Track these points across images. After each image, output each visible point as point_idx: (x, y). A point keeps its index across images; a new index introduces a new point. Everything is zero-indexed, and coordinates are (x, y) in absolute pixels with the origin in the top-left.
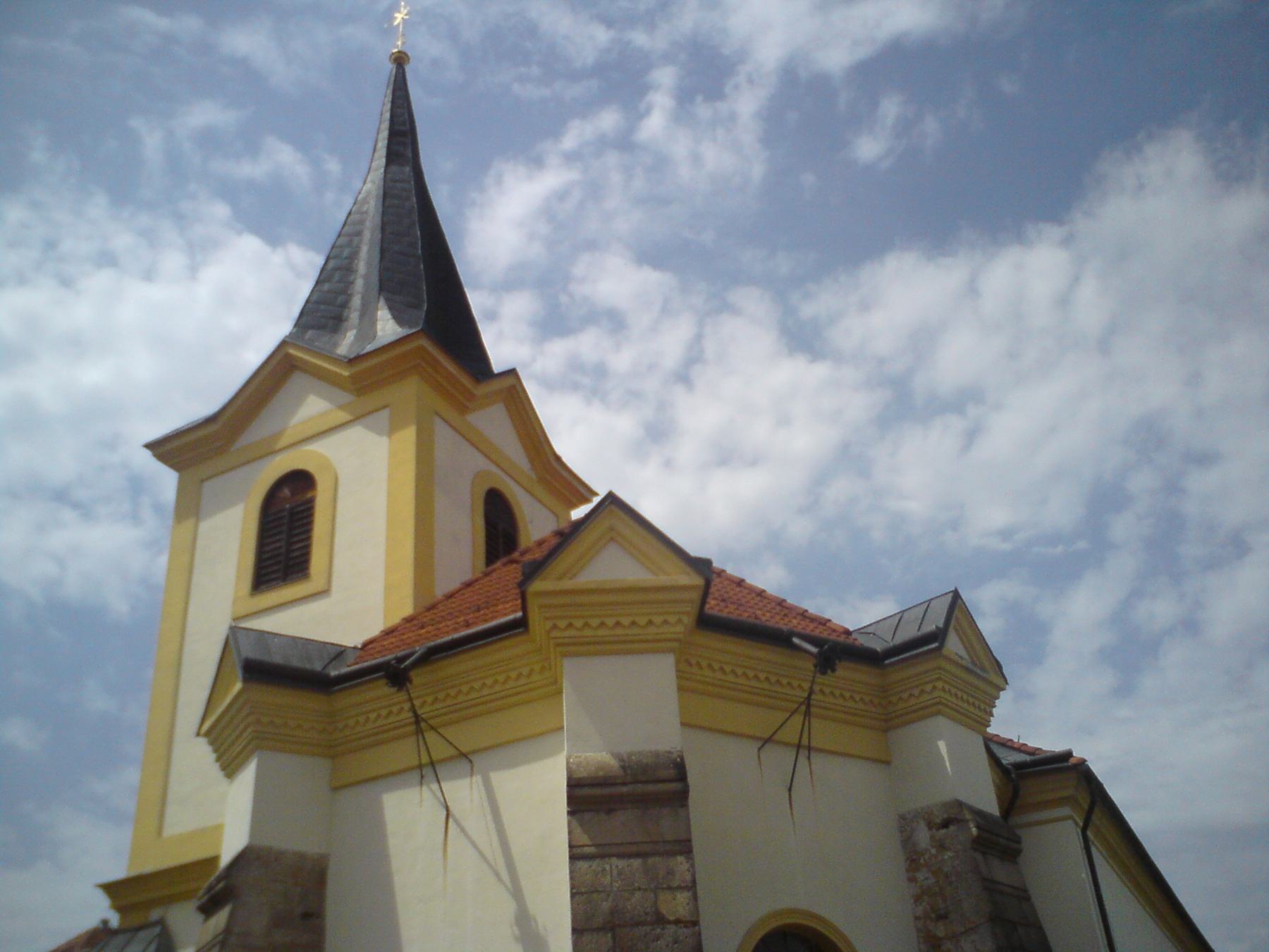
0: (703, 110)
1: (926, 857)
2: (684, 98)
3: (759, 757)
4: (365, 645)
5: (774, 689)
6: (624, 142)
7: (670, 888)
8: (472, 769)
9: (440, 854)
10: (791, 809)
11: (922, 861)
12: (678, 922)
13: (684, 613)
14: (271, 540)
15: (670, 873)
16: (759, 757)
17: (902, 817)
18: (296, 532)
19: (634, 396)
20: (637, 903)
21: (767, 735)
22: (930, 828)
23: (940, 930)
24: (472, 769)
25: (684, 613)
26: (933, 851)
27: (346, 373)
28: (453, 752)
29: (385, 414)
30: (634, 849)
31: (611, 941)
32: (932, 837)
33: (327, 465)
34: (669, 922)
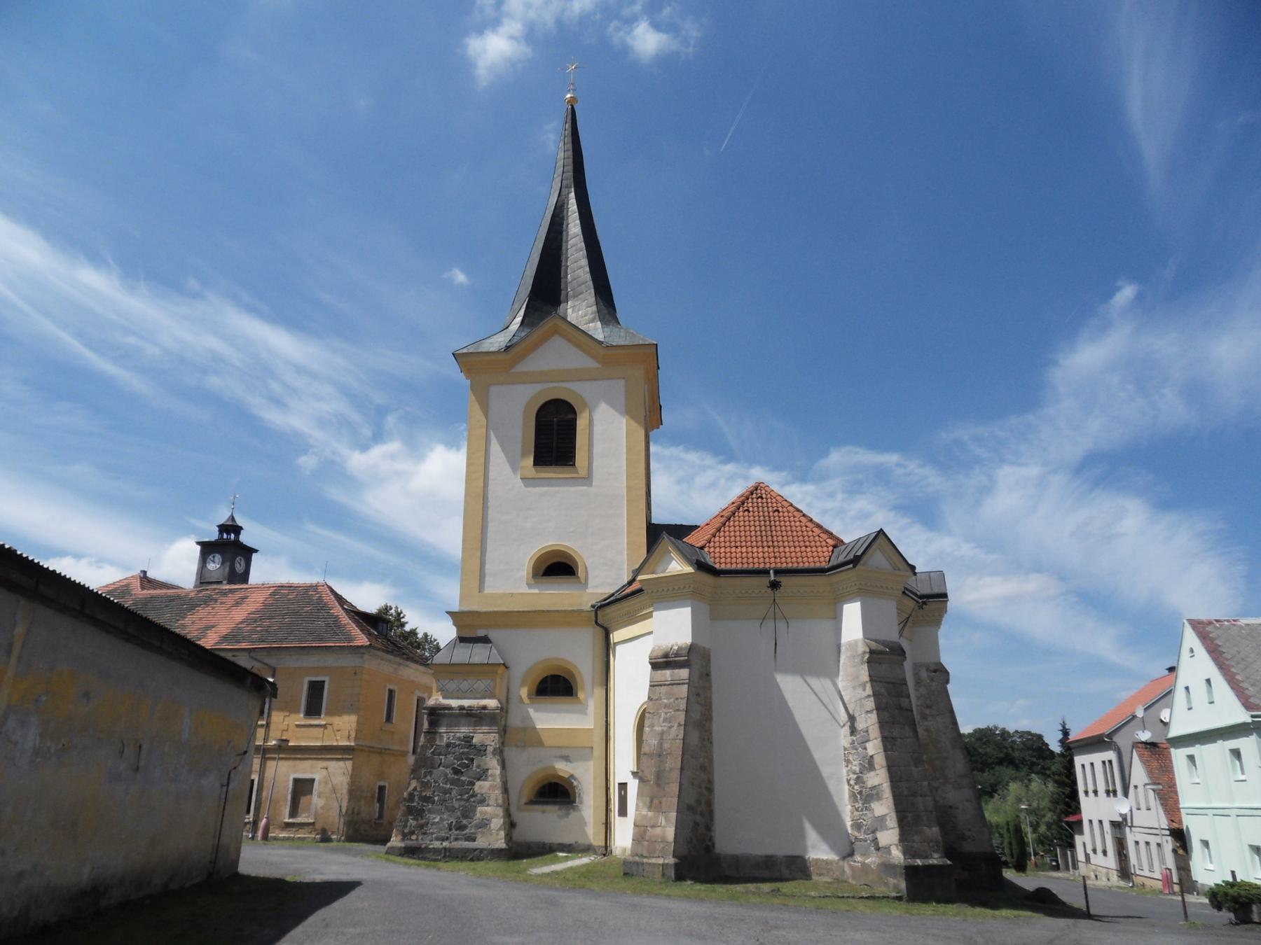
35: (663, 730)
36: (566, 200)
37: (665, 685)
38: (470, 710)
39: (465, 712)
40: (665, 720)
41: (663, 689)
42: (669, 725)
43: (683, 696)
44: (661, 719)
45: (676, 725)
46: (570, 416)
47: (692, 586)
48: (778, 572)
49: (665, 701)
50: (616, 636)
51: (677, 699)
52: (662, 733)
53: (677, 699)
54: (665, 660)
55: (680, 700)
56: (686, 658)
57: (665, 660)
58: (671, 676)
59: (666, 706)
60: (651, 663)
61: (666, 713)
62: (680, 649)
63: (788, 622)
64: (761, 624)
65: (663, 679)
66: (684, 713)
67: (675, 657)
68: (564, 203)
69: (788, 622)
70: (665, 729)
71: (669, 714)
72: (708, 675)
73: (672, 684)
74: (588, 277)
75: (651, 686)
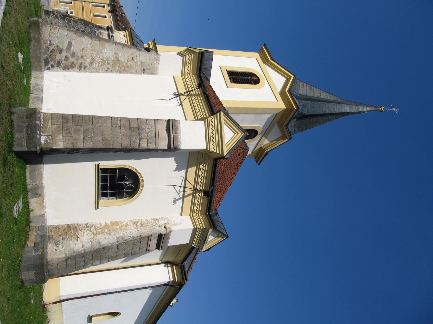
1: (157, 223)
3: (171, 185)
4: (210, 86)
7: (148, 142)
10: (109, 314)
11: (156, 222)
12: (140, 143)
13: (203, 227)
15: (151, 143)
16: (171, 185)
17: (213, 52)
20: (144, 135)
22: (164, 224)
23: (139, 224)
25: (203, 227)
26: (159, 224)
30: (157, 134)
31: (135, 127)
32: (162, 224)
34: (140, 141)
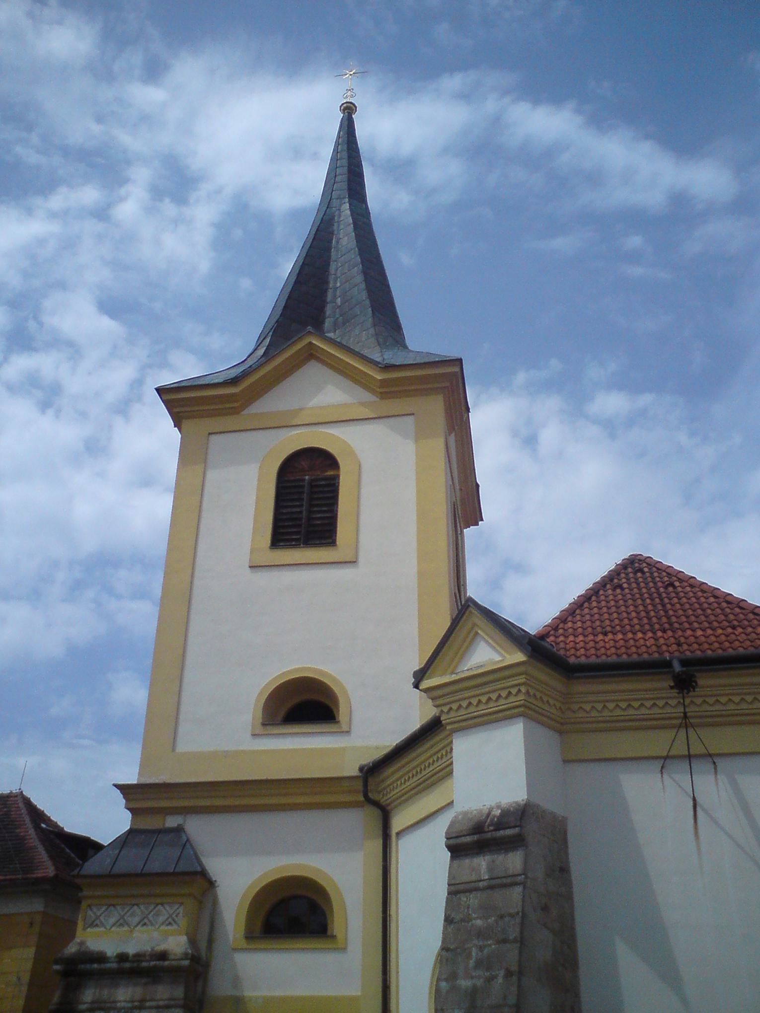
0: (169, 208)
2: (157, 193)
5: (530, 700)
6: (101, 213)
8: (715, 768)
9: (691, 836)
14: (291, 504)
18: (285, 504)
19: (83, 415)
21: (711, 752)
24: (715, 768)
27: (379, 377)
28: (704, 751)
29: (410, 420)
33: (351, 453)
35: (474, 986)
36: (337, 213)
37: (477, 889)
38: (138, 961)
39: (127, 965)
40: (479, 964)
41: (473, 900)
42: (487, 974)
43: (512, 911)
44: (472, 963)
45: (502, 973)
46: (330, 473)
47: (523, 689)
48: (684, 663)
49: (479, 922)
50: (398, 822)
51: (502, 917)
52: (473, 994)
53: (502, 917)
54: (476, 837)
55: (507, 919)
56: (517, 830)
57: (476, 837)
58: (490, 869)
59: (481, 934)
60: (450, 848)
61: (481, 949)
62: (505, 813)
63: (714, 763)
64: (662, 767)
65: (474, 877)
66: (518, 945)
67: (495, 830)
68: (333, 217)
69: (714, 763)
70: (479, 983)
71: (486, 951)
72: (564, 870)
73: (491, 888)
74: (364, 295)
75: (449, 893)
